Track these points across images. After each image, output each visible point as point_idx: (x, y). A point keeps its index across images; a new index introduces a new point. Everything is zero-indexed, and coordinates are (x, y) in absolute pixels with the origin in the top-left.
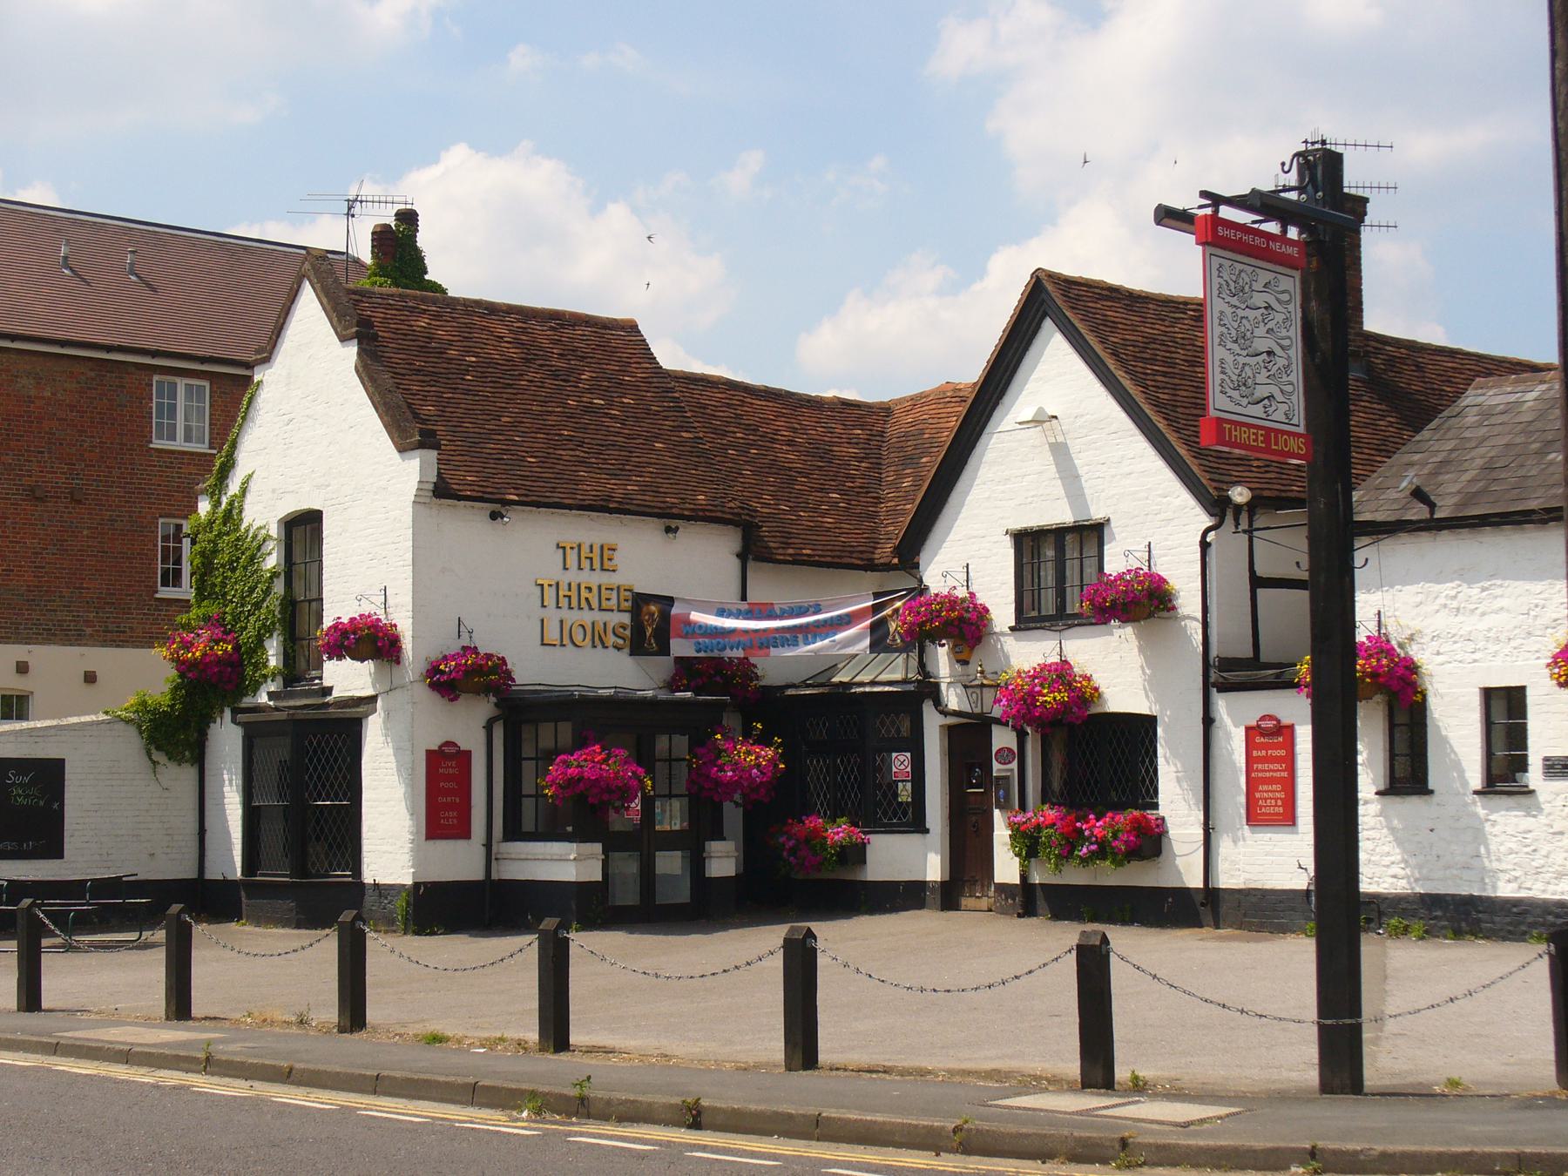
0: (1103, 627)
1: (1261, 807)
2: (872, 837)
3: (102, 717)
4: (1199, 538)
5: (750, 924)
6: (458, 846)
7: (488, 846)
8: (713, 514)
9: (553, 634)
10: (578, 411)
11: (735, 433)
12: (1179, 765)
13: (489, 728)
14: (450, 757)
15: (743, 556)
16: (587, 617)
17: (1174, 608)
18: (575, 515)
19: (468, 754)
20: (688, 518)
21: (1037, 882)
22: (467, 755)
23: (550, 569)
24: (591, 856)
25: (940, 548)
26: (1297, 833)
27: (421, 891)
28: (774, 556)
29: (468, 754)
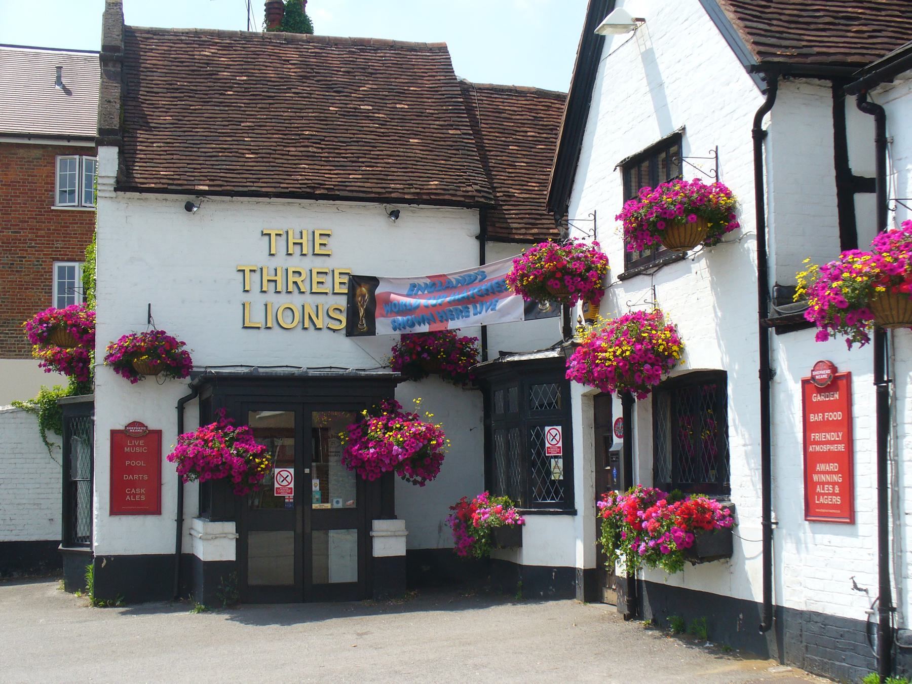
0: (681, 265)
1: (819, 494)
2: (527, 518)
3: (10, 407)
4: (751, 126)
5: (312, 619)
6: (149, 521)
7: (180, 521)
8: (441, 197)
9: (257, 318)
10: (337, 115)
11: (527, 132)
12: (747, 436)
13: (181, 407)
14: (137, 437)
15: (483, 238)
16: (296, 301)
17: (738, 226)
18: (284, 204)
19: (159, 433)
20: (409, 202)
21: (643, 579)
22: (157, 436)
23: (257, 255)
24: (224, 536)
25: (580, 199)
26: (855, 535)
27: (103, 565)
28: (512, 236)
29: (159, 433)
